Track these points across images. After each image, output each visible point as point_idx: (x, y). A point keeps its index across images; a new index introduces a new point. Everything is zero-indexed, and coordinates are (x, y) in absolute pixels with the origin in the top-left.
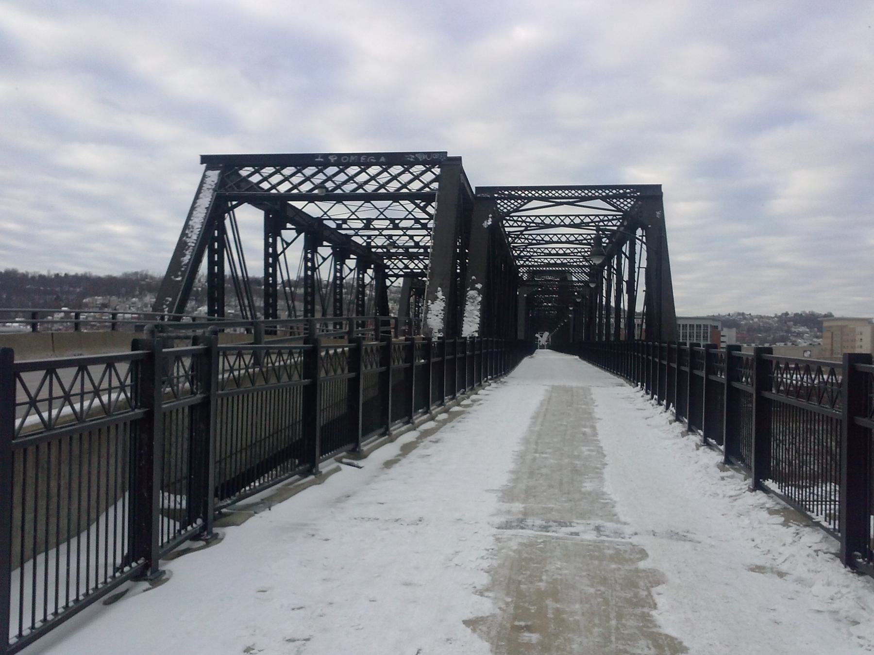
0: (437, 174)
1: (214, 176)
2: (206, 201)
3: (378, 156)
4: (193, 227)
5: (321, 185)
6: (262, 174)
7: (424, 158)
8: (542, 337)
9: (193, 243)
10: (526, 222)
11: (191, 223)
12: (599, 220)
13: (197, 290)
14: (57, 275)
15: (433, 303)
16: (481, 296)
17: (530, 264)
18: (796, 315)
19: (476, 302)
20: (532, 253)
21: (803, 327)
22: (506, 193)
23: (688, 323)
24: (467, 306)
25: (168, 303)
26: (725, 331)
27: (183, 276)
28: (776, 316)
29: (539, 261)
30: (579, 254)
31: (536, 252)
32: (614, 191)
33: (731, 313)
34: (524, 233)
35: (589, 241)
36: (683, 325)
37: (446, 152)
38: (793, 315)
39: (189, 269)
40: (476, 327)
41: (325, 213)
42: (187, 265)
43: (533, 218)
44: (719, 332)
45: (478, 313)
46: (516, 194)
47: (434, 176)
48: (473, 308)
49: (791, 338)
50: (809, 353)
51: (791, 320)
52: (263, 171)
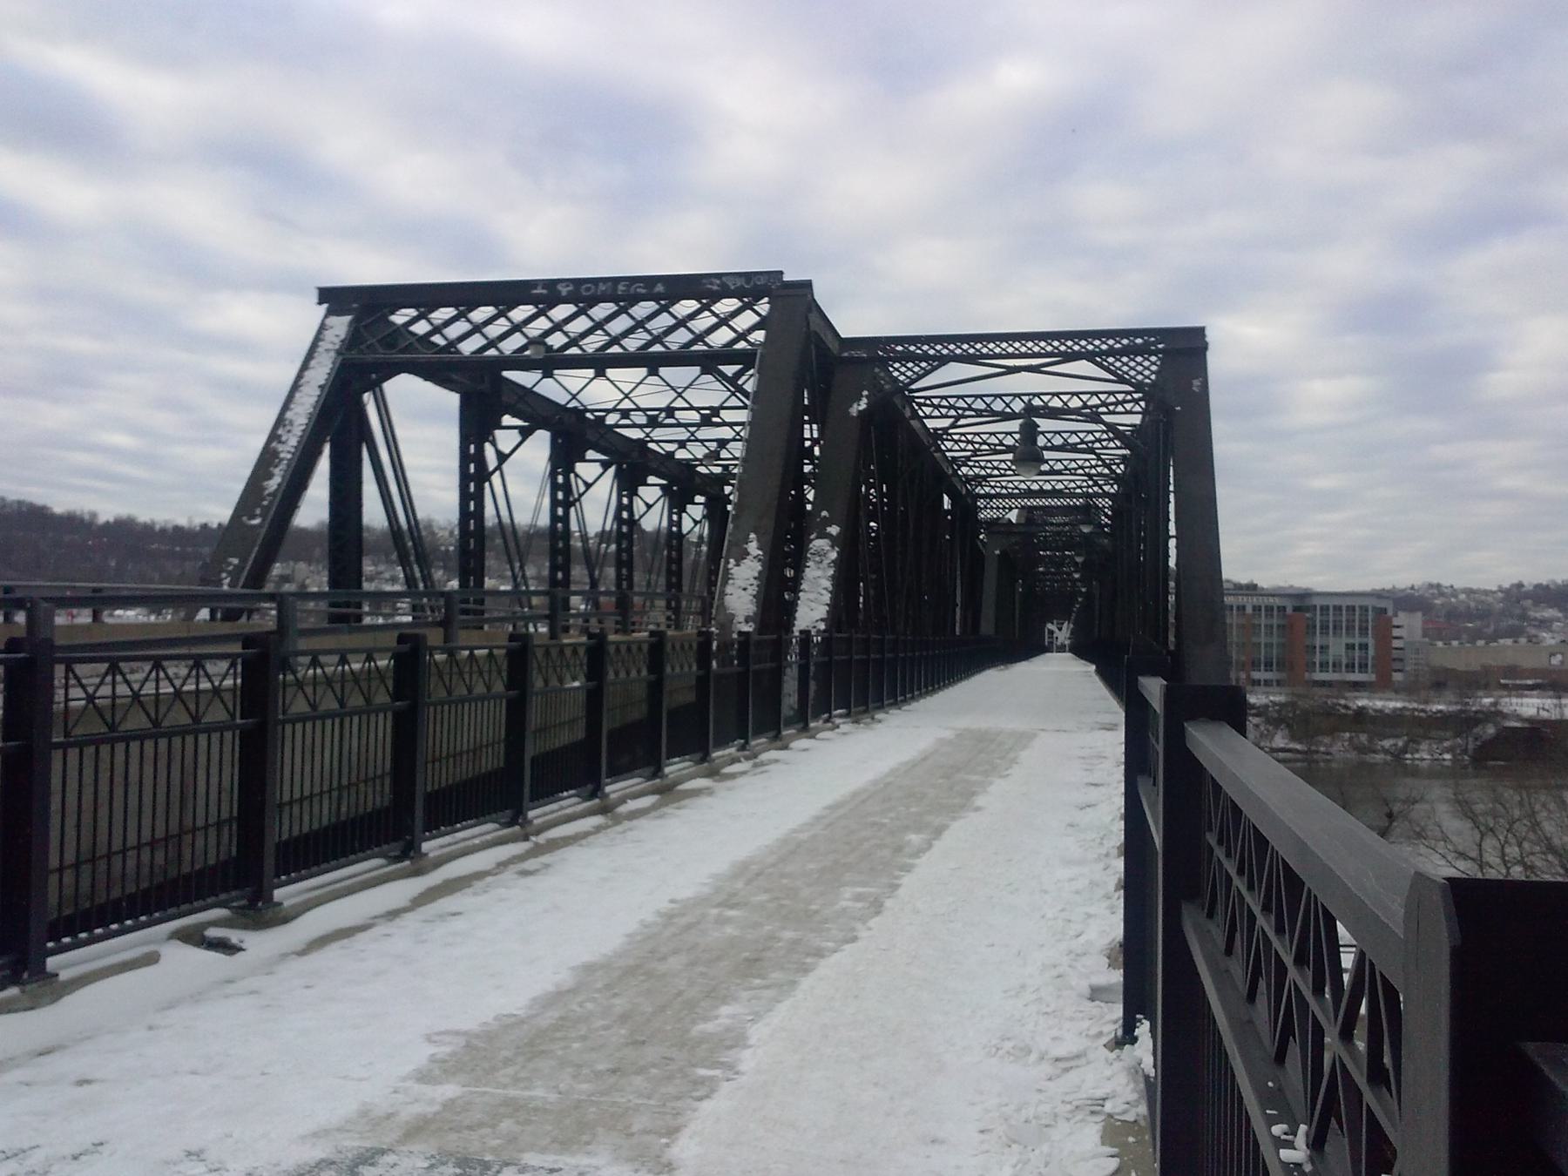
0: (764, 313)
1: (340, 326)
2: (321, 372)
3: (650, 281)
4: (291, 423)
5: (541, 339)
6: (432, 321)
7: (739, 284)
8: (1060, 629)
9: (289, 452)
10: (956, 409)
11: (289, 415)
12: (1114, 400)
13: (447, 551)
14: (205, 526)
15: (738, 565)
16: (837, 549)
17: (993, 492)
18: (1538, 586)
19: (826, 562)
20: (989, 471)
21: (1550, 610)
22: (899, 348)
23: (1332, 602)
24: (807, 569)
25: (231, 568)
26: (1401, 618)
27: (263, 516)
28: (1501, 590)
29: (1010, 485)
30: (1080, 471)
31: (998, 469)
32: (1125, 342)
33: (1415, 584)
34: (951, 431)
35: (1090, 445)
36: (1266, 607)
37: (781, 273)
38: (1531, 588)
39: (276, 504)
40: (822, 611)
41: (626, 396)
42: (274, 494)
43: (969, 400)
44: (1390, 620)
45: (828, 584)
46: (919, 351)
47: (757, 318)
48: (819, 573)
49: (1528, 629)
50: (1559, 657)
51: (1527, 595)
52: (433, 315)
